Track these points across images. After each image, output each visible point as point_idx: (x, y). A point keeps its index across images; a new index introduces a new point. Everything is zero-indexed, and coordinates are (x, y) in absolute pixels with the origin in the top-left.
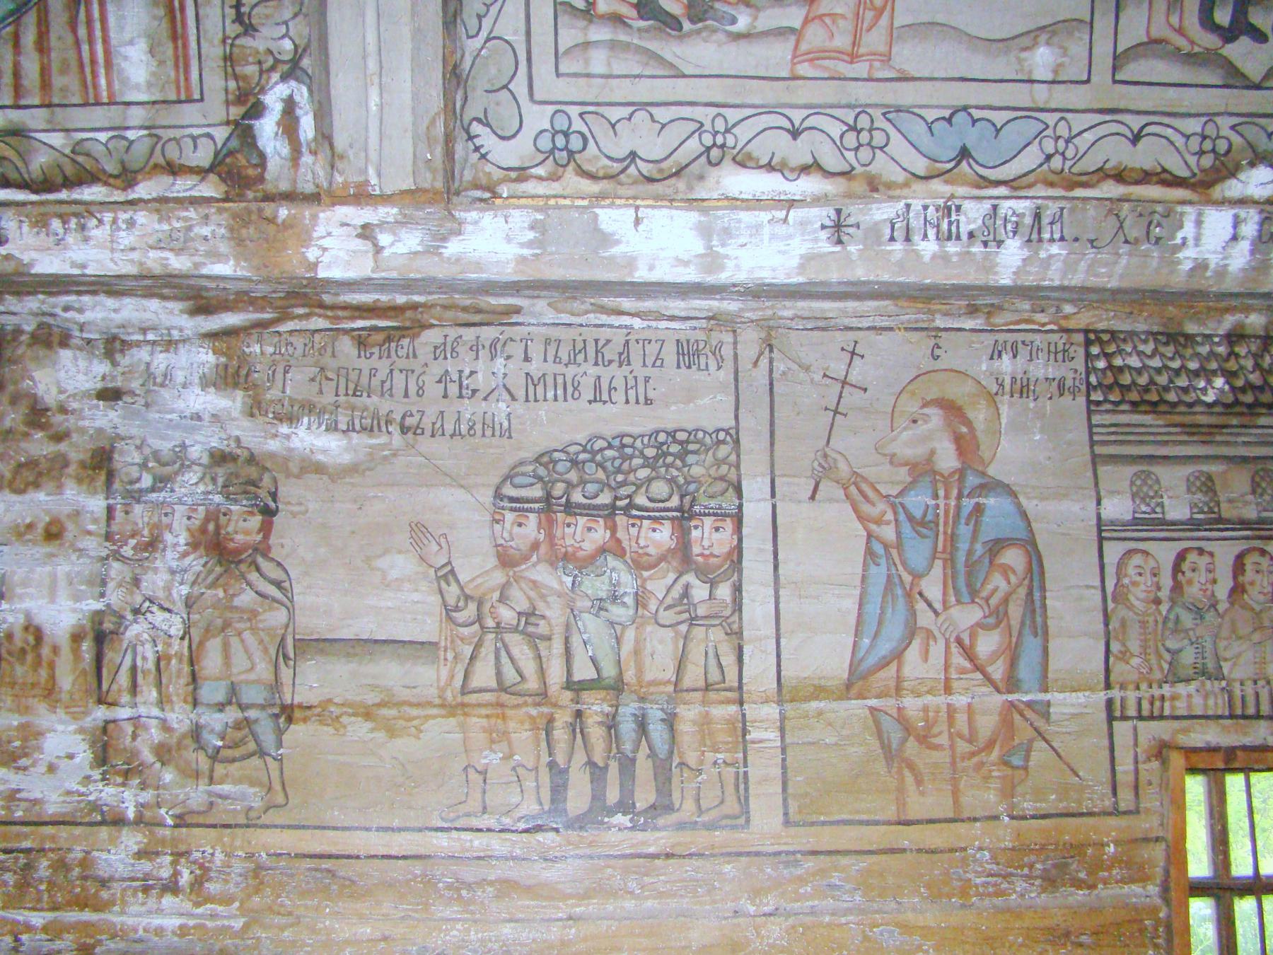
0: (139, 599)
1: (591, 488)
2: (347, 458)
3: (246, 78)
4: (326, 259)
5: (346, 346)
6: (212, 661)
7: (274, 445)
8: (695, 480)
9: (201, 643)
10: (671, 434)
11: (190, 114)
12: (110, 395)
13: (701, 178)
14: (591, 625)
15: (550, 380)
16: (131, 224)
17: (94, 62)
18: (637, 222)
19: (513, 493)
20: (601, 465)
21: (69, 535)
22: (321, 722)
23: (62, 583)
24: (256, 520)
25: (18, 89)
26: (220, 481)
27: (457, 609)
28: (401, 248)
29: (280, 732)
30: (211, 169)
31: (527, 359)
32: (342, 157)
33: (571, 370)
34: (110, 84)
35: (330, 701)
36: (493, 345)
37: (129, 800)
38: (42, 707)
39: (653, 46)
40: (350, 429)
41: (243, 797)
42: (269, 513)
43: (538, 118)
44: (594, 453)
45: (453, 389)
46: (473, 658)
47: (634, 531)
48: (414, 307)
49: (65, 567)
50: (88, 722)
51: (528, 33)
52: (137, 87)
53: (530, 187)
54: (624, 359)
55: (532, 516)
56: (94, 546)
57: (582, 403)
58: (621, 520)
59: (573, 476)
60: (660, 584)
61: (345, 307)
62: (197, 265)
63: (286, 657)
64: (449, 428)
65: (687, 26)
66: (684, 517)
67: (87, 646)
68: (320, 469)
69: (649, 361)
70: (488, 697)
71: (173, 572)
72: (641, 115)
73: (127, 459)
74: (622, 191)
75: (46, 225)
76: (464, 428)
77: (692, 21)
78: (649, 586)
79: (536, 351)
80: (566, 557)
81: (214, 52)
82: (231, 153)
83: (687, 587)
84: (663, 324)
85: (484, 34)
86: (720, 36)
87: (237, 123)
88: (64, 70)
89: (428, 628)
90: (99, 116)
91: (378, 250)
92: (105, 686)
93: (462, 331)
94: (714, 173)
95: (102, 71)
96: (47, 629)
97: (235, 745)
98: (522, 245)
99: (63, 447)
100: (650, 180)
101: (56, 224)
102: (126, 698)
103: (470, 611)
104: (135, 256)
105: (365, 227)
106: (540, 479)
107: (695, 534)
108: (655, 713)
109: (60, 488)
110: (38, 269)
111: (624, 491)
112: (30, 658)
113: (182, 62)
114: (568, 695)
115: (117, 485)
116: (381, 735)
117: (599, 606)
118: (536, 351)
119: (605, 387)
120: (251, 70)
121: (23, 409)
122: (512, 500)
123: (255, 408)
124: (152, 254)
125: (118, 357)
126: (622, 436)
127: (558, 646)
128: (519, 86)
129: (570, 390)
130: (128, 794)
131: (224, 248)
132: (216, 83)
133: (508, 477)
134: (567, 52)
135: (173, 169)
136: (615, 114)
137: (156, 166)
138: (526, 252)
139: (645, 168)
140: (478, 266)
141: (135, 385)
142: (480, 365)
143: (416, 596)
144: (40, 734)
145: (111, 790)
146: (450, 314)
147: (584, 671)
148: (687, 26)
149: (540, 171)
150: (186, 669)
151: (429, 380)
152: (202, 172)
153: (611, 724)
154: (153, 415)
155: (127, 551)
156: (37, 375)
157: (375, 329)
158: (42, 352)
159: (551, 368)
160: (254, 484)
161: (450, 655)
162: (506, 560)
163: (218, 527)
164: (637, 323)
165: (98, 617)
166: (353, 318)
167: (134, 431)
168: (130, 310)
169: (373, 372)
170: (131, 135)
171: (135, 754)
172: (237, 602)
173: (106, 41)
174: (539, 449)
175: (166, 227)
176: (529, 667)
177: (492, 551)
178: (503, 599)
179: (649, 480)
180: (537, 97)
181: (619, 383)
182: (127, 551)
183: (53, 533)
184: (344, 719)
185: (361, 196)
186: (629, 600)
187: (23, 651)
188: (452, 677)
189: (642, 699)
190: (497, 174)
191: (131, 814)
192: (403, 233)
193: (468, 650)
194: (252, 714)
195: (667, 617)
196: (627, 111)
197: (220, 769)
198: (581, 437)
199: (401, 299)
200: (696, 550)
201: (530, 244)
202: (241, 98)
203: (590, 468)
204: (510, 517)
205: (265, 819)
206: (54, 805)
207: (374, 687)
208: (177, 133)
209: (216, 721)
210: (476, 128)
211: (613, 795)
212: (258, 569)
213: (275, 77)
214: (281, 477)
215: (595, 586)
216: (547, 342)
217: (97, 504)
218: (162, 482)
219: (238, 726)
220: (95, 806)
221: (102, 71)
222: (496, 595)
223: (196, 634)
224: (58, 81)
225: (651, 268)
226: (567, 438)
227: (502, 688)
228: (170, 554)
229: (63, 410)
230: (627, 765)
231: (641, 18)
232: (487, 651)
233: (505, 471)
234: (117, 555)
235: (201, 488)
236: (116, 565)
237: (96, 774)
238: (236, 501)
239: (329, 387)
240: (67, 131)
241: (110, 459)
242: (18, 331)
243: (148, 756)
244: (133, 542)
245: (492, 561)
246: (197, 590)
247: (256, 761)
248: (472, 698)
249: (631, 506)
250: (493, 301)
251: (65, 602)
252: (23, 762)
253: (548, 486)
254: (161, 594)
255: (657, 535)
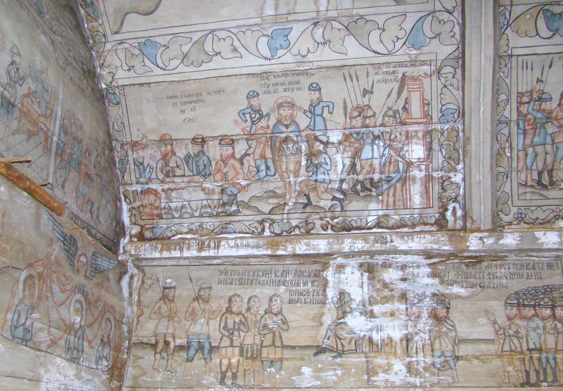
0: (417, 330)
1: (529, 300)
2: (467, 294)
3: (444, 202)
4: (471, 245)
5: (463, 267)
6: (437, 346)
7: (448, 291)
8: (555, 297)
9: (434, 341)
10: (548, 286)
11: (430, 211)
12: (404, 280)
13: (554, 223)
14: (532, 334)
15: (516, 274)
16: (424, 237)
17: (406, 199)
18: (544, 234)
19: (509, 302)
20: (531, 294)
21: (396, 315)
22: (466, 360)
23: (396, 326)
24: (445, 310)
25: (387, 205)
26: (435, 301)
27: (498, 331)
28: (489, 242)
29: (455, 363)
30: (435, 224)
31: (509, 269)
32: (475, 221)
33: (521, 271)
34: (410, 204)
35: (468, 355)
36: (501, 265)
37: (418, 381)
38: (393, 358)
39: (541, 192)
40: (467, 287)
41: (447, 380)
42: (448, 308)
43: (514, 210)
44: (529, 291)
45: (492, 277)
46: (504, 343)
47: (541, 311)
48: (481, 256)
49: (396, 323)
50: (405, 362)
51: (511, 190)
52: (417, 205)
53: (513, 226)
54: (534, 268)
55: (515, 308)
56: (403, 317)
57: (524, 279)
58: (537, 308)
59: (524, 297)
60: (549, 324)
61: (463, 257)
62: (440, 247)
63: (456, 344)
64: (492, 286)
65: (549, 187)
66: (553, 307)
67: (404, 342)
68: (460, 297)
69: (540, 268)
70: (507, 353)
71: (425, 323)
72: (539, 209)
73: (410, 295)
74: (534, 227)
75: (404, 238)
76: (495, 286)
77: (551, 186)
78: (546, 324)
79: (511, 267)
80: (525, 318)
81: (436, 196)
82: (440, 220)
83: (556, 324)
84: (543, 259)
85: (501, 191)
86: (557, 189)
87: (441, 213)
88: (399, 200)
89: (492, 336)
90: (407, 211)
91: (484, 243)
92: (409, 352)
93: (493, 262)
94: (557, 222)
95: (409, 201)
96: (394, 338)
97: (443, 367)
98: (518, 241)
99: (393, 293)
100: (542, 224)
101: (406, 238)
102: (415, 355)
103: (502, 331)
104: (425, 245)
105: (481, 237)
106: (516, 298)
107: (556, 311)
108: (550, 356)
109: (393, 303)
110: (399, 249)
111: (537, 301)
112: (389, 346)
113: (428, 198)
114: (528, 352)
115: (408, 302)
116: (481, 363)
117: (534, 330)
118: (511, 267)
119: (529, 275)
120: (445, 200)
121: (381, 283)
122: (509, 304)
123: (442, 282)
124: (429, 245)
125: (405, 270)
126: (535, 287)
127: (525, 340)
128: (510, 203)
129: (521, 276)
130: (417, 380)
131: (447, 243)
132: (436, 204)
133: (508, 298)
134: (521, 194)
135: (425, 224)
136: (533, 208)
137: (421, 223)
138: (518, 242)
139: (540, 221)
140: (507, 246)
141: (410, 277)
142: (498, 271)
143: (488, 328)
144: (392, 365)
145: (412, 379)
146: (490, 258)
147: (532, 346)
148: (549, 187)
149: (515, 223)
150: (430, 347)
151: (485, 274)
152: (432, 225)
153: (539, 359)
154: (415, 284)
155: (412, 318)
156: (384, 275)
157: (471, 262)
158: (384, 269)
159: (516, 271)
160: (444, 301)
161: (498, 342)
162: (510, 319)
163: (435, 312)
164: (536, 259)
165: (406, 335)
166: (465, 259)
167: (411, 289)
168: (409, 258)
169: (471, 273)
170: (415, 216)
171: (418, 369)
172: (442, 330)
173: (410, 194)
174: (515, 291)
175: (433, 238)
176: (518, 345)
177: (505, 317)
178: (510, 328)
179: (543, 298)
180: (514, 205)
181: (533, 274)
182: (412, 318)
183: (392, 314)
184: (472, 360)
185: (478, 230)
186: (541, 328)
187: (387, 344)
188: (498, 348)
189: (547, 353)
190: (504, 224)
191: (418, 384)
192: (489, 239)
193: (502, 341)
194: (448, 359)
195: (551, 332)
196: (536, 208)
197: (440, 373)
198: (525, 288)
199: (478, 254)
200: (557, 315)
201: (519, 241)
202: (442, 207)
203: (528, 295)
204: (509, 308)
205: (453, 385)
206: (398, 382)
207: (479, 351)
208: (426, 215)
209: (438, 360)
210: (499, 213)
211: (542, 378)
212: (446, 322)
213: (451, 202)
214: (451, 299)
215: (532, 325)
216: (514, 264)
217: (403, 307)
218: (420, 301)
219: (444, 362)
220: (409, 383)
221: (409, 201)
222: (508, 327)
223: (432, 338)
224: (397, 203)
225: (547, 245)
226: (521, 288)
227: (511, 351)
228: (423, 319)
229: (392, 283)
230: (545, 370)
231: (538, 186)
232: (507, 341)
233: (507, 296)
234: (410, 320)
235: (430, 302)
236: (410, 322)
237: (408, 375)
238: (439, 306)
239: (460, 277)
240: (399, 215)
241: (406, 296)
242: (377, 264)
243: (421, 370)
244: (413, 316)
245: (506, 319)
246: (431, 328)
247: (450, 371)
248: (504, 353)
249: (540, 304)
250: (501, 254)
251: (397, 331)
252: (389, 372)
253: (518, 300)
254: (422, 329)
255: (547, 312)
